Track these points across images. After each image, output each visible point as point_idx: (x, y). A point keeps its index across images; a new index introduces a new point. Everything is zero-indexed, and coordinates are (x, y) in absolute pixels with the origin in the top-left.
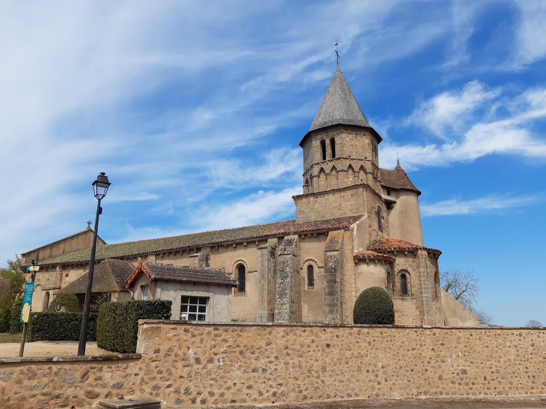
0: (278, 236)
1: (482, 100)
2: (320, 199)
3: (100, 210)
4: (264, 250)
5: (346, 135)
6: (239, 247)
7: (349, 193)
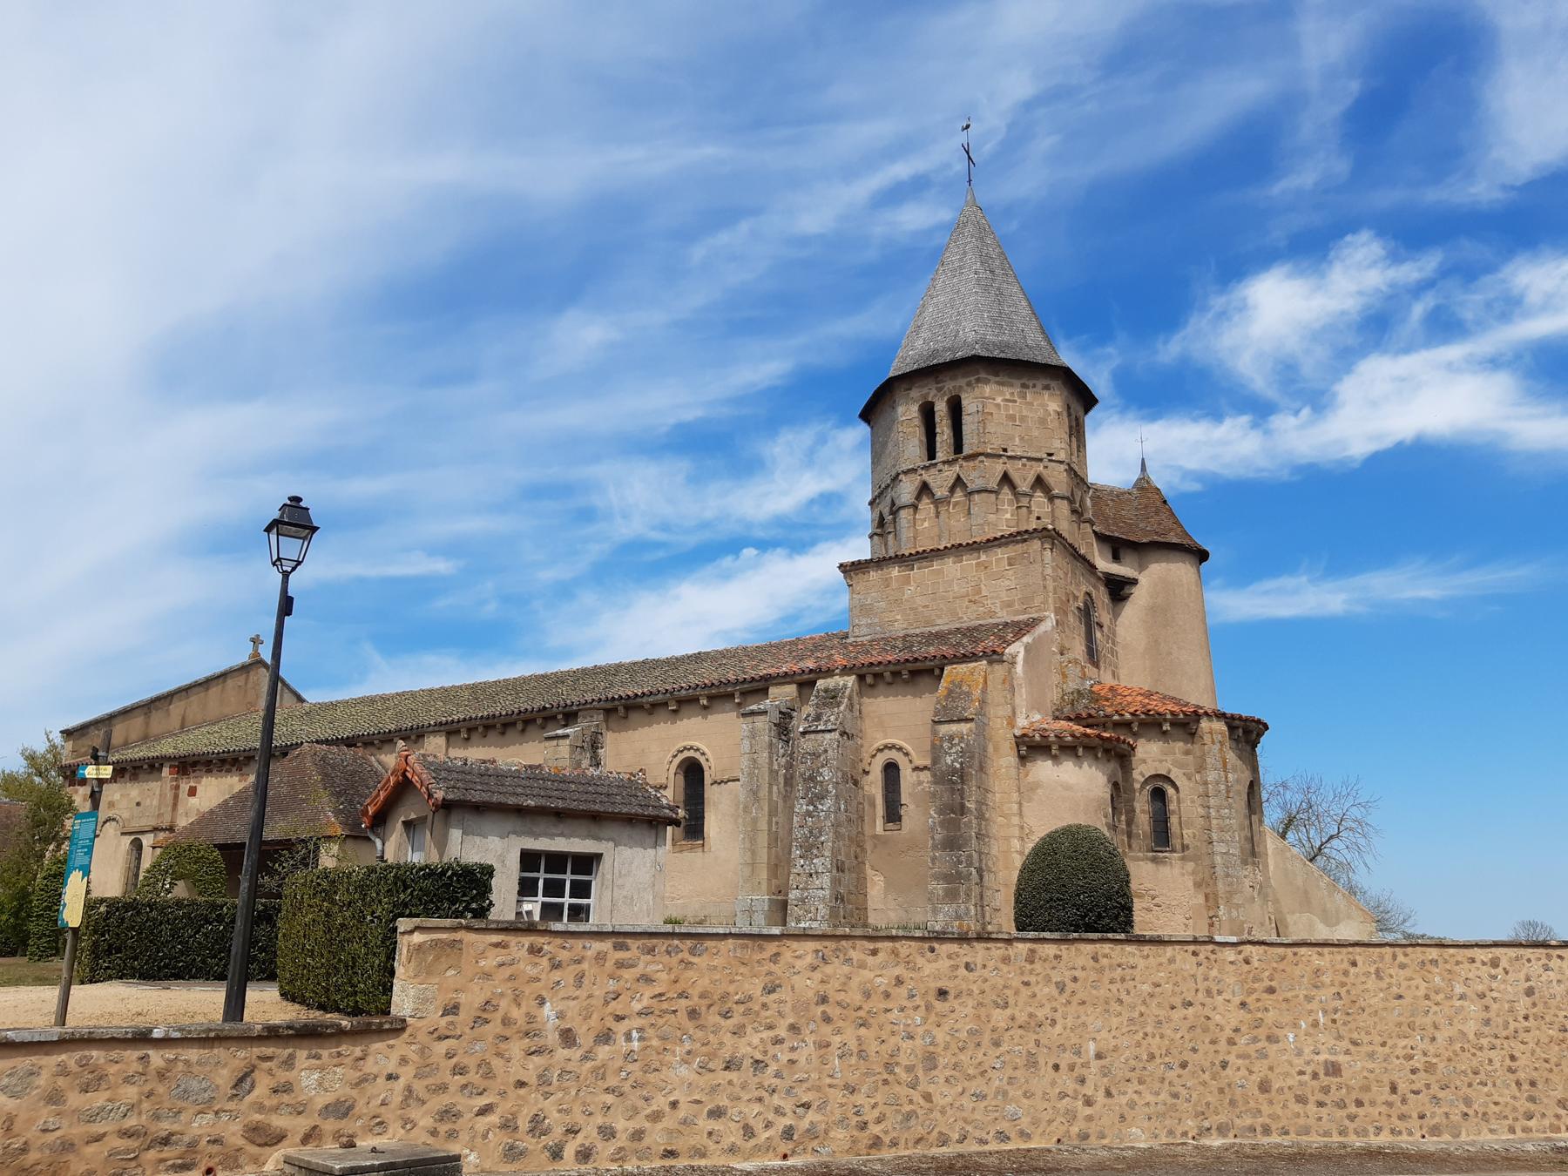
0: (798, 678)
1: (1384, 288)
2: (918, 573)
3: (286, 605)
4: (757, 718)
5: (995, 387)
6: (685, 709)
7: (1001, 554)
